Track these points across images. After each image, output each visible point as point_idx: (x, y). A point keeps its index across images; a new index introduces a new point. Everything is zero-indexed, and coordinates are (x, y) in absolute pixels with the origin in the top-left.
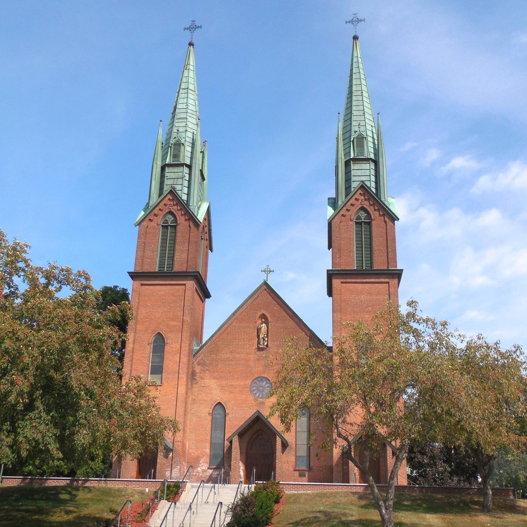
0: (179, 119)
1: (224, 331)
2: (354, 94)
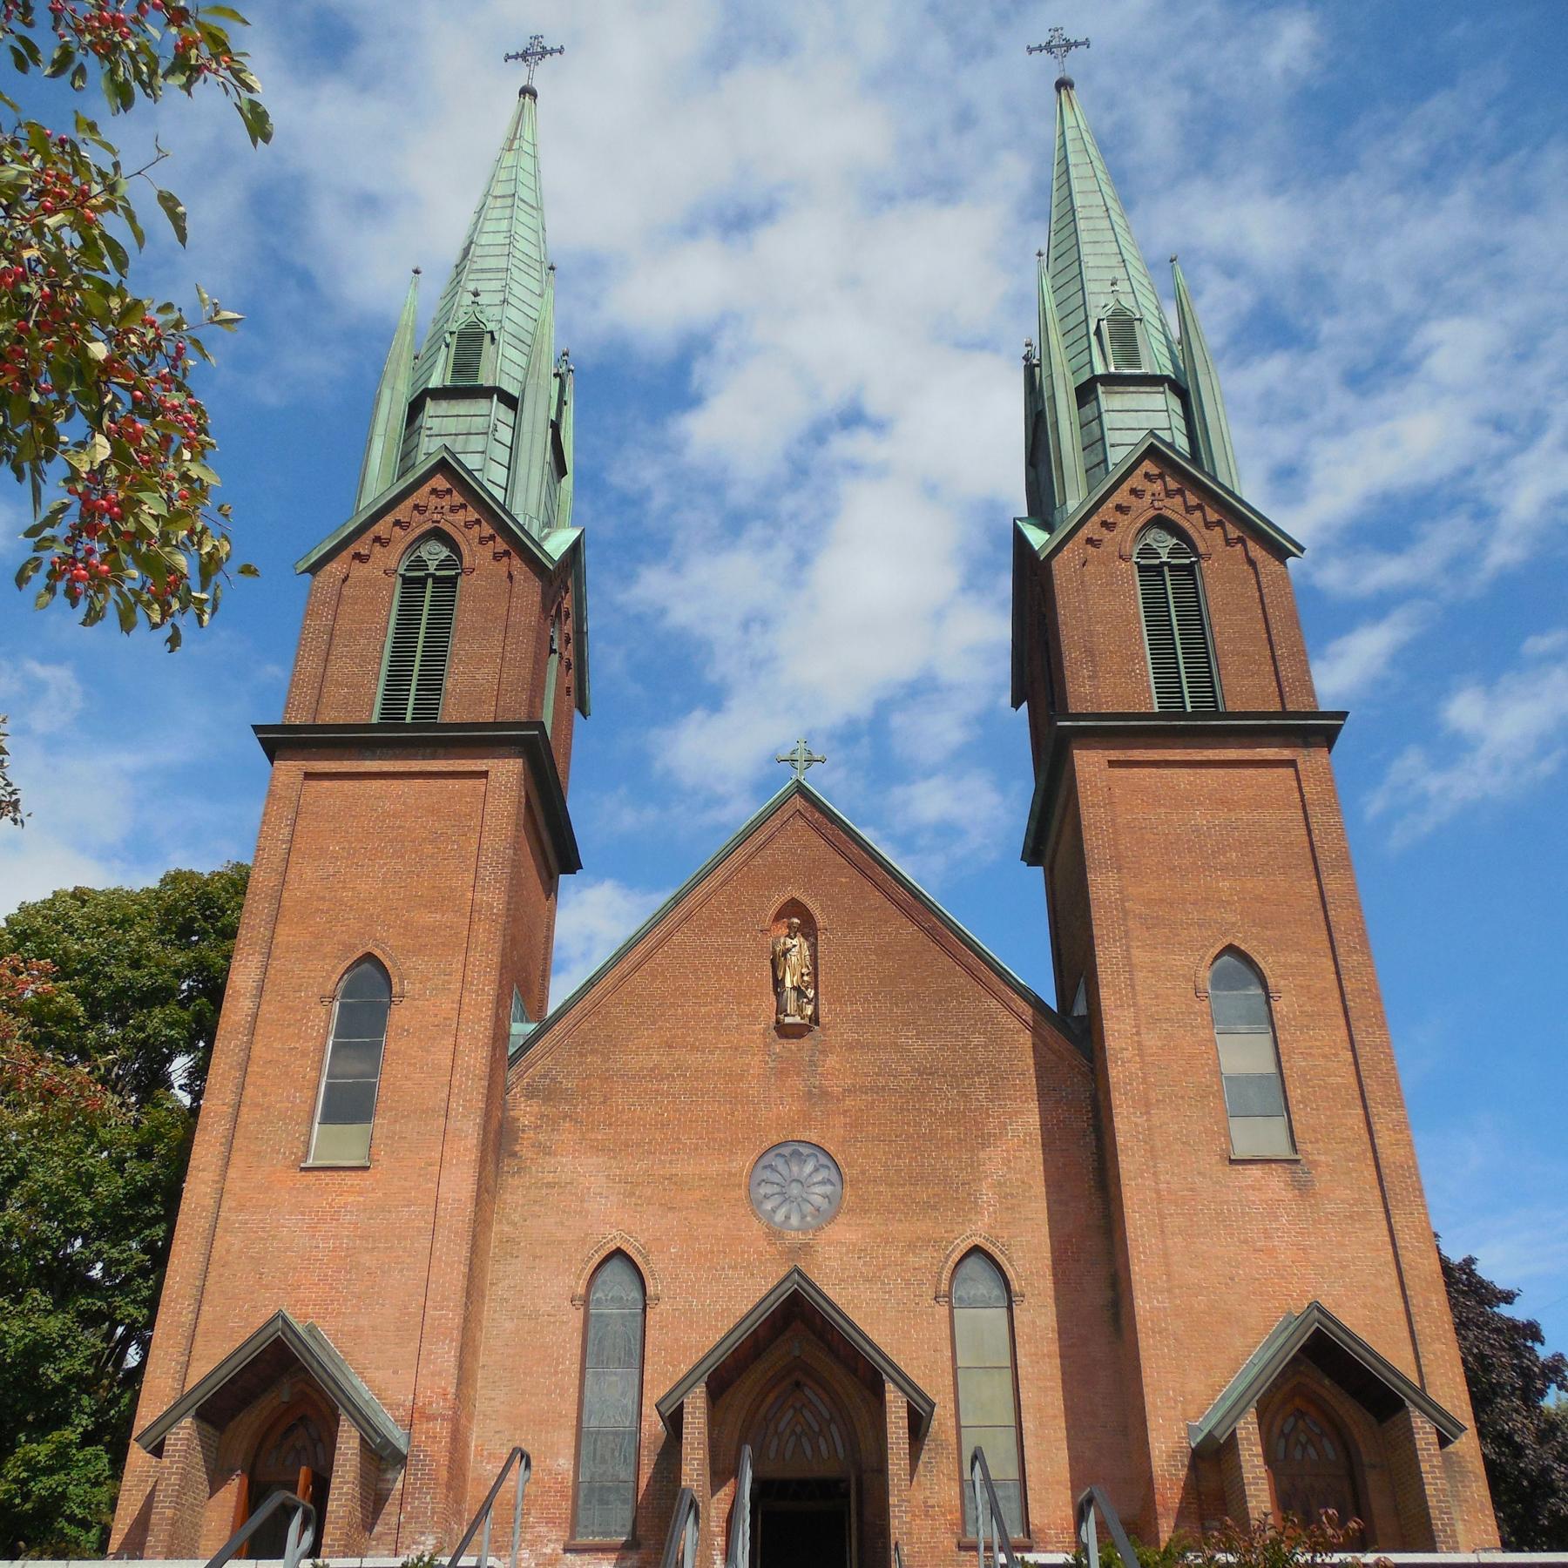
0: (482, 271)
2: (1078, 215)
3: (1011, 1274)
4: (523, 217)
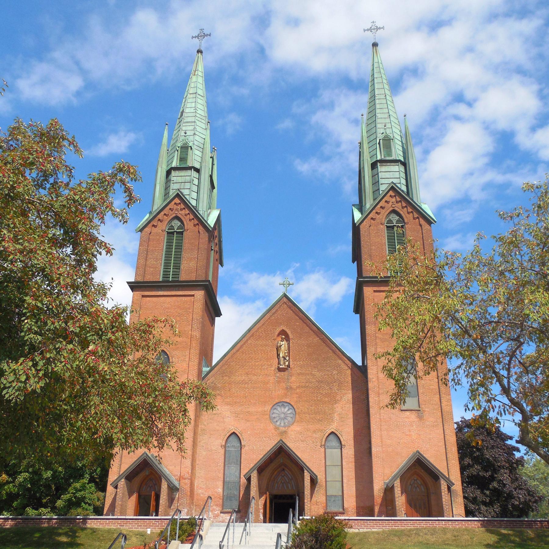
0: (187, 122)
1: (238, 351)
2: (376, 98)
3: (342, 440)
4: (199, 101)
